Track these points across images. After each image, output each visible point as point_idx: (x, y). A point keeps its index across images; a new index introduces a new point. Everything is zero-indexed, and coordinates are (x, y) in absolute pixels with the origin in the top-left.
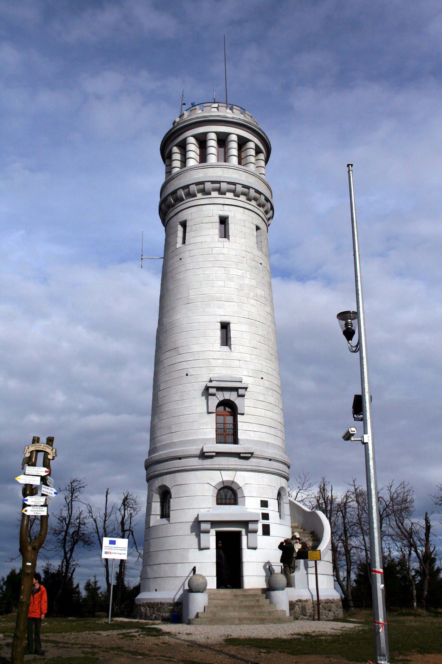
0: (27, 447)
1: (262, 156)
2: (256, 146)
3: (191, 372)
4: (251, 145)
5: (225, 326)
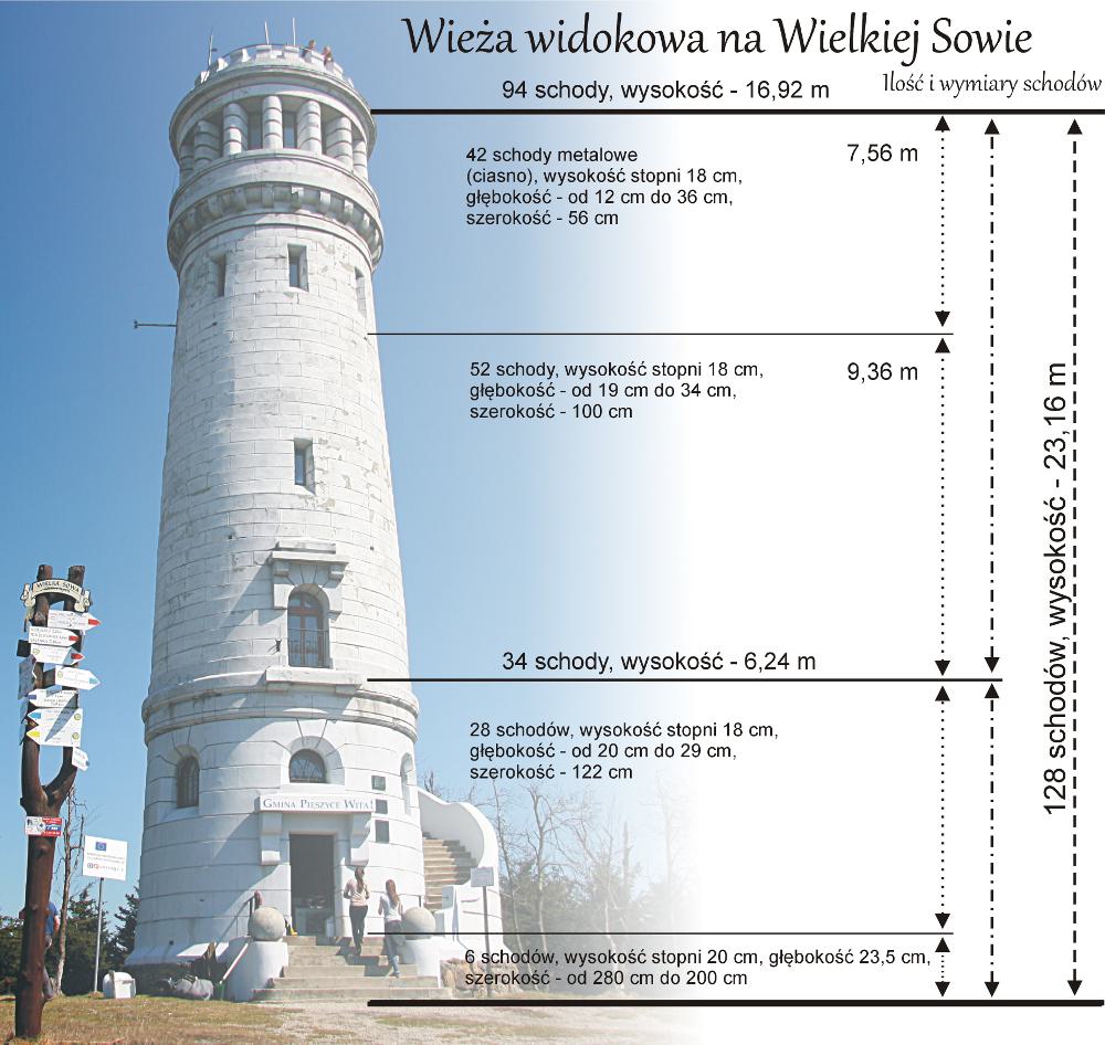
0: (27, 587)
1: (363, 146)
2: (353, 124)
3: (239, 531)
4: (345, 123)
5: (302, 451)
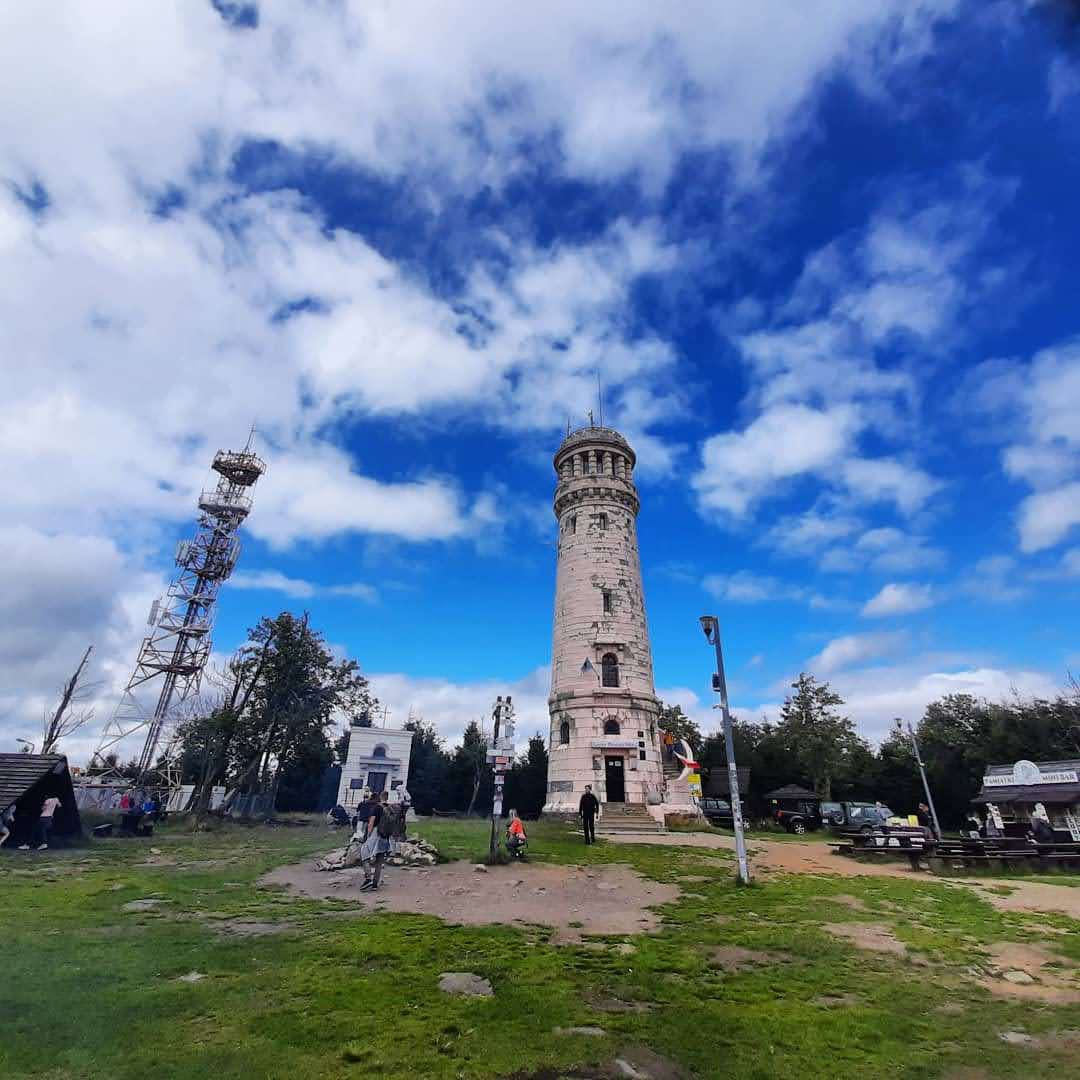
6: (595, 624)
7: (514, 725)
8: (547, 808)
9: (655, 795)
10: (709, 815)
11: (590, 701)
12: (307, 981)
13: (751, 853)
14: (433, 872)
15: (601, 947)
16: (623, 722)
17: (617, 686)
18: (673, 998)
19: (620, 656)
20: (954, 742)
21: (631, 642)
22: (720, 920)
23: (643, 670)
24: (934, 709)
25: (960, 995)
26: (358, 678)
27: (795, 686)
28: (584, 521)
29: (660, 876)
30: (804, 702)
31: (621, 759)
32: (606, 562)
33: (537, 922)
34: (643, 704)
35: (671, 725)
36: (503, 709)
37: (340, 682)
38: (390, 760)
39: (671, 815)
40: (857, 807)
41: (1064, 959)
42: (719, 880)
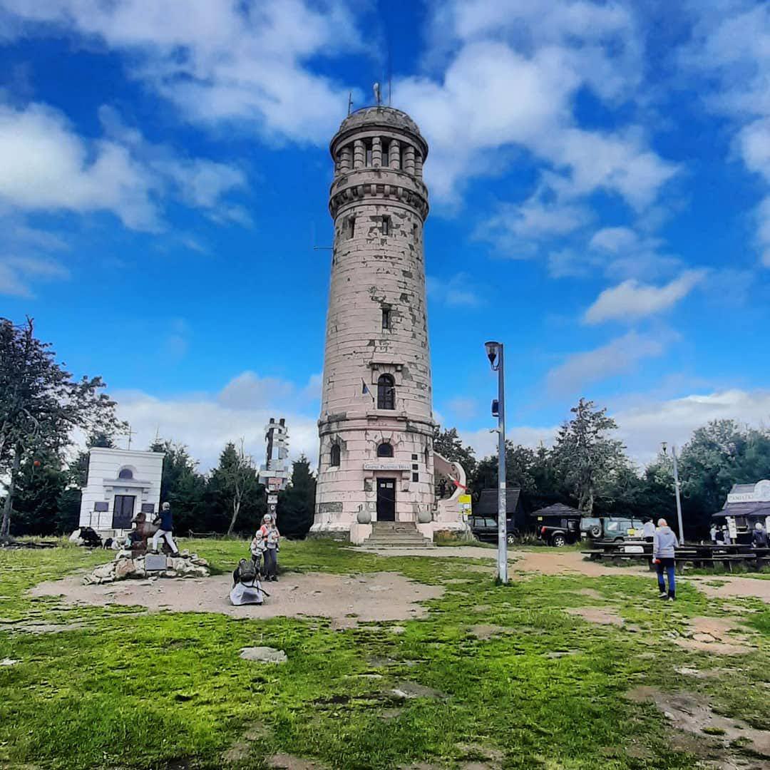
1: (420, 159)
2: (415, 150)
6: (372, 343)
7: (287, 447)
8: (314, 528)
9: (424, 512)
10: (477, 532)
11: (364, 424)
12: (120, 659)
13: (511, 562)
14: (207, 583)
15: (376, 629)
16: (397, 445)
17: (393, 409)
18: (436, 656)
19: (398, 378)
20: (712, 463)
21: (410, 363)
22: (478, 608)
23: (421, 392)
24: (700, 433)
25: (656, 648)
26: (103, 397)
27: (574, 410)
28: (363, 224)
29: (428, 580)
30: (581, 426)
31: (393, 481)
32: (387, 272)
33: (318, 615)
34: (419, 426)
35: (445, 445)
36: (276, 431)
37: (81, 400)
38: (137, 482)
39: (440, 531)
40: (615, 521)
41: (745, 628)
42: (481, 582)
